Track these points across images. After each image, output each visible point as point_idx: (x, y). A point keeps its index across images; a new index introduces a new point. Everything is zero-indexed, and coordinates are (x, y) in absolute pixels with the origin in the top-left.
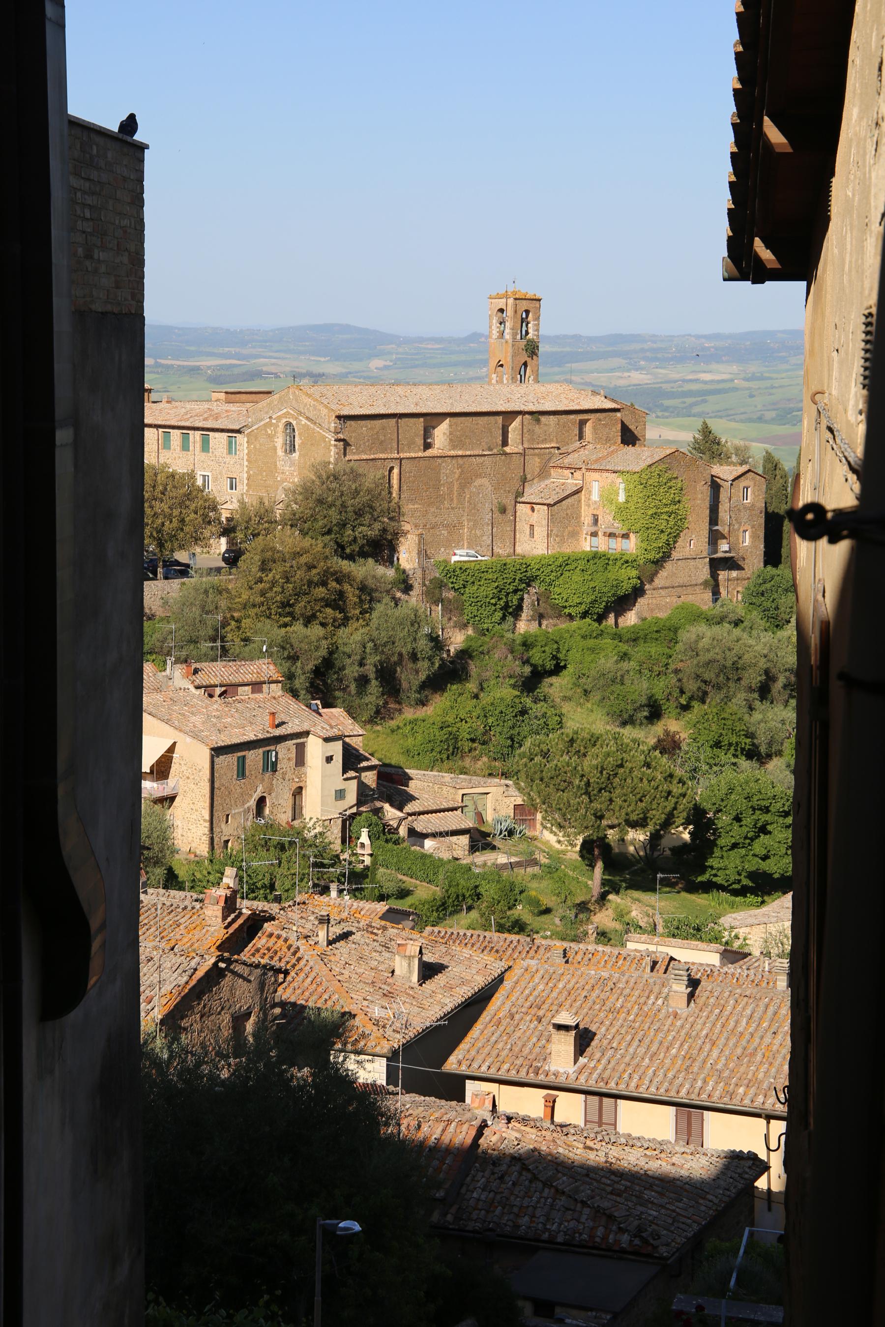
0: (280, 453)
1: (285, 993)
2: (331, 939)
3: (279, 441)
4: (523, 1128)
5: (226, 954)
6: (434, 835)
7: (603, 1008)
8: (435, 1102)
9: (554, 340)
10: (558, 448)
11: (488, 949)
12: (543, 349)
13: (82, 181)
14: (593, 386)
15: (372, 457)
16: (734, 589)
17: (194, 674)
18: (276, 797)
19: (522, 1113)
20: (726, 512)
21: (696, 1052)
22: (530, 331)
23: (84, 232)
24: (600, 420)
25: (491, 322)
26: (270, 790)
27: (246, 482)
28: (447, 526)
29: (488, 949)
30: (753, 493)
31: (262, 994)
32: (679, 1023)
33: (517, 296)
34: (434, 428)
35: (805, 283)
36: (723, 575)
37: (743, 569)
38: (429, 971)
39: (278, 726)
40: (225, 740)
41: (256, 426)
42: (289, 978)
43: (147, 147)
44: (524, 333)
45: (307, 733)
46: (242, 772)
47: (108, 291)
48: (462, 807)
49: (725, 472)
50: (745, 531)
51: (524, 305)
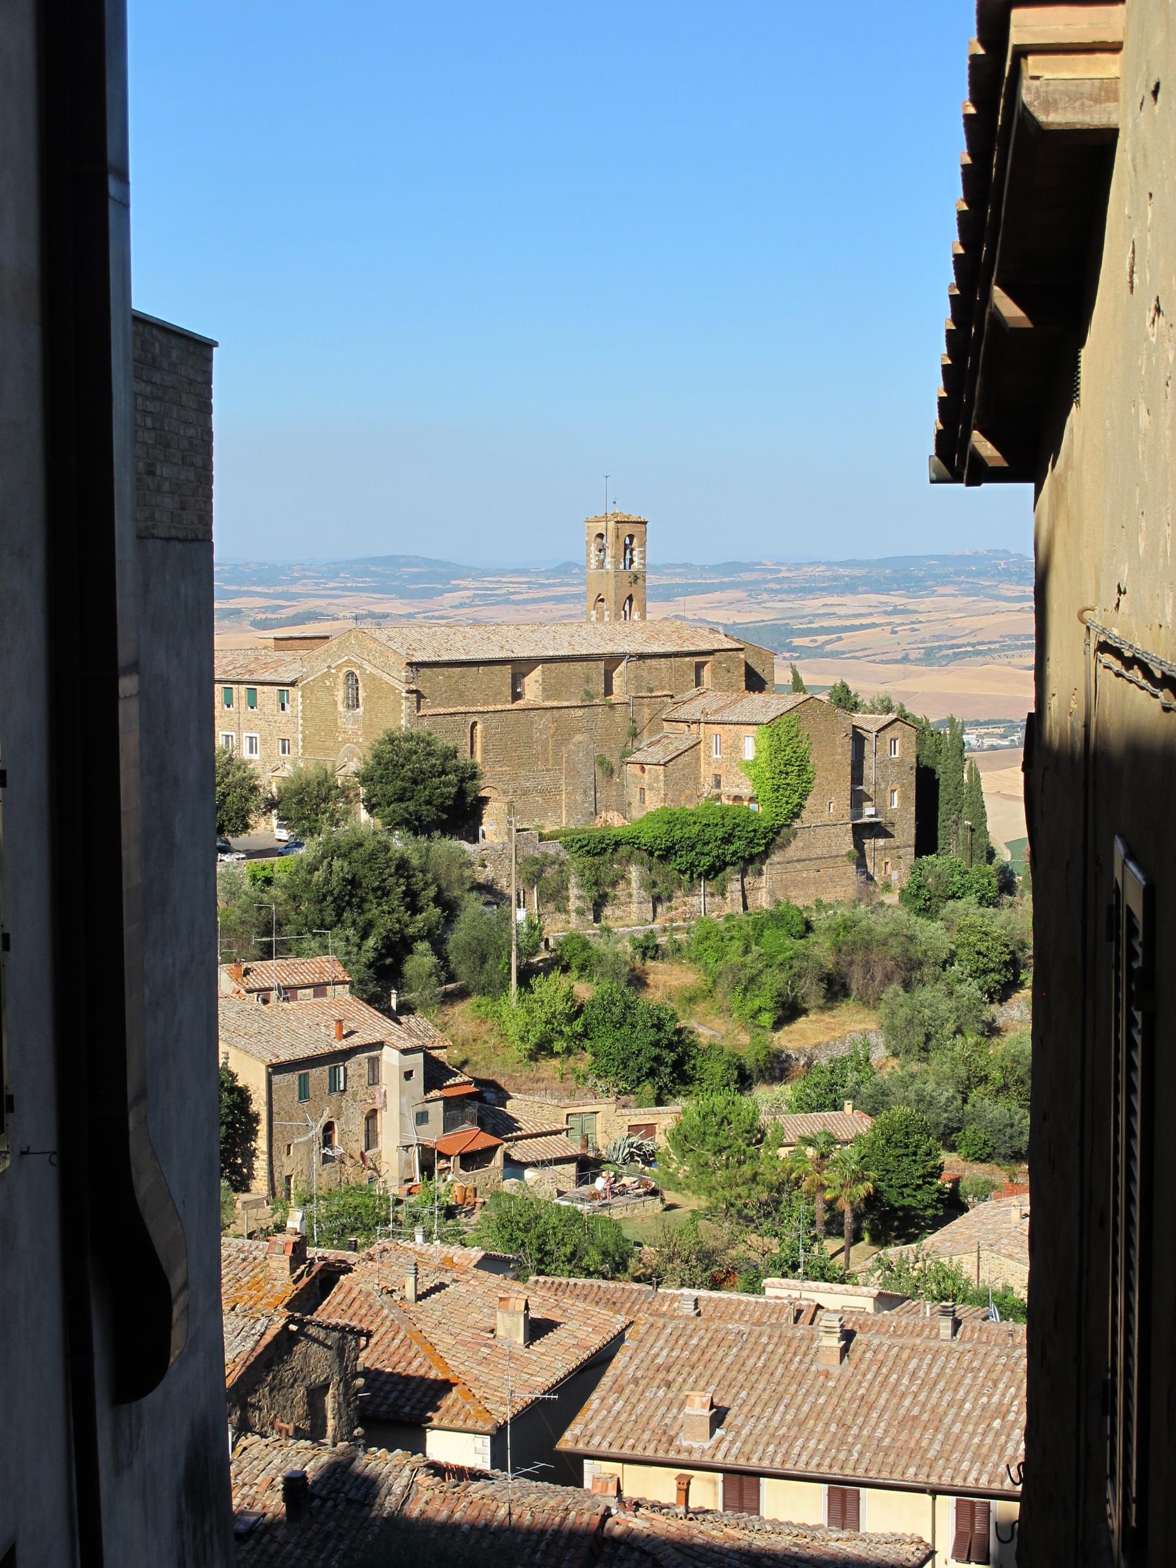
0: (341, 708)
1: (366, 1359)
2: (420, 1293)
3: (340, 695)
4: (653, 1515)
5: (297, 1314)
6: (534, 1164)
7: (743, 1369)
8: (549, 1488)
9: (659, 570)
10: (672, 697)
11: (604, 1300)
12: (651, 580)
13: (143, 384)
14: (709, 622)
15: (451, 710)
16: (882, 860)
17: (245, 975)
18: (346, 1122)
19: (651, 1497)
20: (871, 768)
21: (850, 1418)
22: (635, 559)
23: (146, 444)
24: (720, 663)
25: (588, 549)
26: (339, 1114)
27: (301, 743)
28: (542, 792)
29: (604, 1300)
30: (902, 745)
31: (341, 1362)
32: (831, 1384)
33: (619, 519)
34: (524, 675)
35: (1031, 486)
36: (869, 844)
37: (893, 836)
38: (537, 1329)
39: (345, 1036)
40: (285, 1056)
41: (312, 678)
42: (373, 1341)
43: (216, 344)
44: (628, 562)
45: (380, 1045)
46: (304, 1095)
47: (172, 513)
48: (567, 1130)
49: (868, 722)
50: (893, 791)
51: (627, 529)
